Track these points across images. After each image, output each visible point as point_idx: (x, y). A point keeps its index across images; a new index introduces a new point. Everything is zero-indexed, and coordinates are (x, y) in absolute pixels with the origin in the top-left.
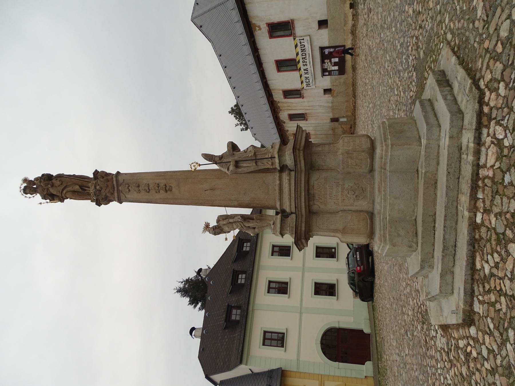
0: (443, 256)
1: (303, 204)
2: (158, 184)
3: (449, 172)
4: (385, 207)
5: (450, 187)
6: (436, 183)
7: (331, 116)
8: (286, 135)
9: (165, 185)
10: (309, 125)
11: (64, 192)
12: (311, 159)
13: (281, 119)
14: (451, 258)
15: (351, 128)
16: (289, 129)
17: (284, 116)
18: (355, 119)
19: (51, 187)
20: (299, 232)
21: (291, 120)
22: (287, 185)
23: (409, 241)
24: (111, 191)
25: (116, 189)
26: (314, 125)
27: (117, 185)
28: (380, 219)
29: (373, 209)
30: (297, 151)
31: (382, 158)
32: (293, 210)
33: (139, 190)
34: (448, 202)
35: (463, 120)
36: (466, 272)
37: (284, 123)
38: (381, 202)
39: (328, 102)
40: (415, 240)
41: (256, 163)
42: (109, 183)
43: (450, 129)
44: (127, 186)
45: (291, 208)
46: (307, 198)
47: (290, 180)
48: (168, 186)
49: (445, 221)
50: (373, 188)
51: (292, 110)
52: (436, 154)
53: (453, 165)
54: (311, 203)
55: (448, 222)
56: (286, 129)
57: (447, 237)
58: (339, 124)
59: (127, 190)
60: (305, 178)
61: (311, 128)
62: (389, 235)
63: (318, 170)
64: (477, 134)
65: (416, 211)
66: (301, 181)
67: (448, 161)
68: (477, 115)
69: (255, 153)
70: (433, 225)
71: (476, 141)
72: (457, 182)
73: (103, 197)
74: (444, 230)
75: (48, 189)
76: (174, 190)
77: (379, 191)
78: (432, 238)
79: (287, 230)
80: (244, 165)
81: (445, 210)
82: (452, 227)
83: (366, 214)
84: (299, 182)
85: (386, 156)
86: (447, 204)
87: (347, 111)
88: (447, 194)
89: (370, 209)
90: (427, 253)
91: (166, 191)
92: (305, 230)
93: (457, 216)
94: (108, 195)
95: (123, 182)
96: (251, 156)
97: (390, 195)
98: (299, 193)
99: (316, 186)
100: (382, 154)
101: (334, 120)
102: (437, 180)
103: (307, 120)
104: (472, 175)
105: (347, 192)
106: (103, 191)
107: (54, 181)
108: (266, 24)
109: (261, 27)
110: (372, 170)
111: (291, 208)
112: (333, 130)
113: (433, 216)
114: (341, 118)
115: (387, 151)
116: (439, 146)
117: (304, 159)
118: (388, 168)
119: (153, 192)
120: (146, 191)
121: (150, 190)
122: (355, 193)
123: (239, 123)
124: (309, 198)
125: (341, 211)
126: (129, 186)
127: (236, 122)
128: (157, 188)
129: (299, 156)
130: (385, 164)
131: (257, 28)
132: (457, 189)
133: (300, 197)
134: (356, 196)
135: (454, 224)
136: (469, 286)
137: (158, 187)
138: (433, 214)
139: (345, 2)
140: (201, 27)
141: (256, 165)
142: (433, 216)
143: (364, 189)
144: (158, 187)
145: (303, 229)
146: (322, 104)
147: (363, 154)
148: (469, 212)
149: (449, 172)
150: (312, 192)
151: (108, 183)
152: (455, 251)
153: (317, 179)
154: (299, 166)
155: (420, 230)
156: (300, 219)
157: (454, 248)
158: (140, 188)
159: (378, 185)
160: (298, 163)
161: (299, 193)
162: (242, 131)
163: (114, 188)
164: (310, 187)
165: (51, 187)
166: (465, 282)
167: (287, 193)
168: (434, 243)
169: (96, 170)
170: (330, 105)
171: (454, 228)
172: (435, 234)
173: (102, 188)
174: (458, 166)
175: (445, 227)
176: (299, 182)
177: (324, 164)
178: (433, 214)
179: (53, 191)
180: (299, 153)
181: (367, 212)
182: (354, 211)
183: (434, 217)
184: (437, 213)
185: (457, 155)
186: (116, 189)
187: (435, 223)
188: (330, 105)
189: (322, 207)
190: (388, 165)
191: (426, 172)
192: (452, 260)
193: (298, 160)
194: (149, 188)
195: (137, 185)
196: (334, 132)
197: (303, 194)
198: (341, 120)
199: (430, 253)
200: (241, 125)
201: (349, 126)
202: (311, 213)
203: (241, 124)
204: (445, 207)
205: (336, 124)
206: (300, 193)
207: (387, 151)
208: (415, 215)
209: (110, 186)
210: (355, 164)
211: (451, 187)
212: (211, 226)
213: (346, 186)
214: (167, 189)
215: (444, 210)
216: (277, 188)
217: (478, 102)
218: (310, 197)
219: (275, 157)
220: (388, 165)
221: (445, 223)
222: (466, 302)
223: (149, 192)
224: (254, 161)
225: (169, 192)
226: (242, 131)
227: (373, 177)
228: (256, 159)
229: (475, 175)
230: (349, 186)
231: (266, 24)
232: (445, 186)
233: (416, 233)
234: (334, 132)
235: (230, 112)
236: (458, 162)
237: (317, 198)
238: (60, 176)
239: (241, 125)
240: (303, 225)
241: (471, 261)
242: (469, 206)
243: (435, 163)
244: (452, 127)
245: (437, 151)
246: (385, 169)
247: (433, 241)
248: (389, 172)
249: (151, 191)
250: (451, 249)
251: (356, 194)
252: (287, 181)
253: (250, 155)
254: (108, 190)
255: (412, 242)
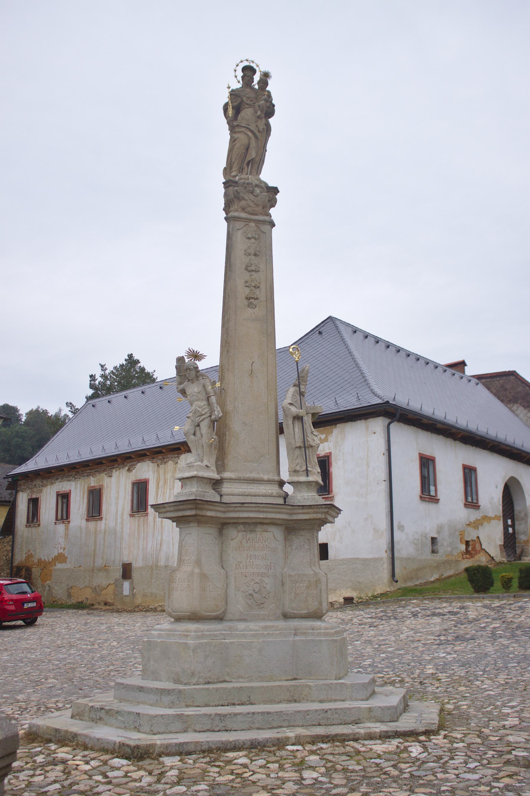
0: (210, 715)
1: (246, 515)
2: (258, 287)
3: (327, 712)
4: (244, 636)
5: (308, 715)
6: (295, 701)
7: (138, 564)
8: (100, 472)
9: (257, 299)
10: (119, 520)
11: (250, 134)
12: (303, 529)
13: (139, 465)
14: (209, 727)
15: (106, 604)
16: (114, 479)
17: (145, 470)
18: (131, 611)
19: (250, 108)
20: (206, 507)
21: (134, 484)
22: (264, 491)
23: (200, 673)
24: (249, 209)
25: (253, 217)
26: (118, 529)
27: (258, 221)
28: (222, 630)
29: (231, 620)
30: (325, 510)
31: (313, 629)
32: (225, 499)
33: (250, 255)
34: (287, 715)
35: (390, 721)
36: (213, 742)
37: (129, 470)
38: (251, 630)
39: (167, 559)
40: (201, 680)
41: (300, 447)
42: (259, 209)
43: (380, 707)
44: (257, 237)
45: (229, 495)
46: (250, 521)
47: (271, 496)
48: (255, 302)
49: (262, 713)
50: (264, 619)
51: (158, 488)
52: (333, 697)
53: (337, 715)
54: (241, 527)
55: (260, 718)
56: (115, 473)
57: (239, 717)
58: (116, 580)
59: (250, 236)
60: (279, 519)
61: (111, 524)
62: (206, 643)
63: (285, 540)
64: (391, 734)
65: (240, 680)
66: (279, 513)
67: (341, 709)
68: (412, 731)
69: (312, 446)
70: (236, 702)
71: (383, 734)
72: (314, 723)
73: (242, 195)
74: (248, 713)
75: (250, 106)
76: (250, 310)
77: (266, 628)
78: (217, 703)
79: (198, 487)
80: (297, 430)
81: (277, 712)
82: (253, 723)
83: (223, 609)
84: (278, 510)
85: (319, 634)
86: (284, 714)
87: (144, 596)
88: (299, 712)
89: (229, 616)
90: (193, 697)
91: (248, 298)
92: (207, 516)
93: (269, 728)
94: (243, 203)
95: (261, 231)
96: (308, 441)
97: (263, 642)
98: (264, 509)
99: (265, 534)
100: (320, 629)
101: (127, 571)
102: (299, 702)
103: (131, 516)
104: (343, 735)
105: (258, 581)
106: (251, 197)
107: (264, 121)
108: (330, 453)
109: (325, 444)
110: (286, 616)
111: (229, 495)
112: (105, 569)
113: (249, 701)
114: (132, 584)
115: (326, 635)
116: (343, 701)
117: (310, 520)
118: (297, 638)
119: (247, 276)
120: (247, 266)
121: (250, 271)
122: (256, 593)
123: (107, 372)
124: (249, 524)
125: (227, 572)
126: (255, 239)
127: (110, 368)
128: (253, 284)
129: (317, 513)
130: (304, 634)
131: (323, 437)
132: (304, 724)
133: (259, 511)
134: (251, 595)
135: (257, 725)
136: (192, 748)
137: (255, 287)
138: (251, 701)
139: (354, 589)
140: (320, 333)
141: (297, 447)
142: (249, 701)
143: (262, 606)
144: (255, 287)
145: (209, 514)
146: (164, 547)
147: (316, 603)
148: (296, 737)
149: (327, 712)
150: (259, 529)
151: (261, 207)
152: (219, 731)
153: (275, 535)
154: (301, 511)
155: (211, 686)
156: (221, 509)
157: (224, 729)
158: (253, 257)
159: (273, 626)
160: (307, 511)
161: (264, 509)
162: (91, 376)
163: (252, 214)
164: (265, 527)
165: (250, 108)
166: (197, 742)
167: (252, 491)
168: (209, 706)
169: (278, 192)
170: (162, 563)
171: (252, 726)
172: (222, 705)
173: (256, 196)
174: (335, 722)
175: (253, 713)
176: (278, 510)
177: (294, 547)
178: (251, 701)
179: (247, 113)
180: (322, 513)
181: (225, 612)
182: (226, 591)
183: (248, 703)
184: (254, 706)
185: (348, 720)
186: (253, 217)
187: (239, 705)
188: (162, 563)
189: (233, 544)
190: (303, 638)
191: (310, 687)
192: (205, 729)
193: (310, 510)
194: (253, 271)
195: (258, 253)
196: (100, 570)
197: (261, 516)
198: (126, 585)
199: (193, 702)
200: (102, 376)
201: (109, 600)
202: (222, 526)
203: (103, 376)
204: (281, 712)
205: (119, 574)
206: (263, 512)
207: (326, 635)
208: (233, 680)
209: (256, 209)
210: (298, 592)
211: (308, 717)
212: (197, 362)
213: (266, 580)
214: (251, 300)
215: (267, 710)
216: (254, 475)
217: (426, 730)
218: (251, 525)
219: (307, 476)
220: (303, 638)
221: (259, 713)
222: (167, 747)
223: (246, 269)
224: (302, 445)
225: (246, 302)
226: (91, 376)
227: (277, 619)
228: (305, 447)
229: (343, 738)
230: (267, 584)
231: (330, 453)
232: (308, 709)
233: (209, 683)
234: (100, 570)
235: (130, 356)
236: (339, 721)
237: (249, 536)
238: (268, 129)
239: (102, 376)
240: (212, 514)
241: (228, 747)
242: (304, 736)
243: (322, 697)
244: (382, 709)
245: (338, 698)
246: (295, 635)
247: (211, 704)
248: (293, 641)
249: (248, 274)
250: (221, 725)
251: (255, 595)
252: (270, 491)
253: (309, 440)
254: (251, 204)
255: (199, 678)
